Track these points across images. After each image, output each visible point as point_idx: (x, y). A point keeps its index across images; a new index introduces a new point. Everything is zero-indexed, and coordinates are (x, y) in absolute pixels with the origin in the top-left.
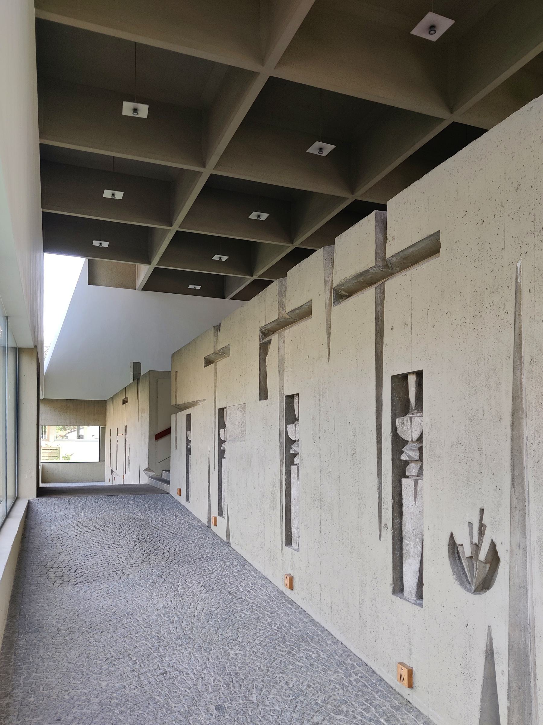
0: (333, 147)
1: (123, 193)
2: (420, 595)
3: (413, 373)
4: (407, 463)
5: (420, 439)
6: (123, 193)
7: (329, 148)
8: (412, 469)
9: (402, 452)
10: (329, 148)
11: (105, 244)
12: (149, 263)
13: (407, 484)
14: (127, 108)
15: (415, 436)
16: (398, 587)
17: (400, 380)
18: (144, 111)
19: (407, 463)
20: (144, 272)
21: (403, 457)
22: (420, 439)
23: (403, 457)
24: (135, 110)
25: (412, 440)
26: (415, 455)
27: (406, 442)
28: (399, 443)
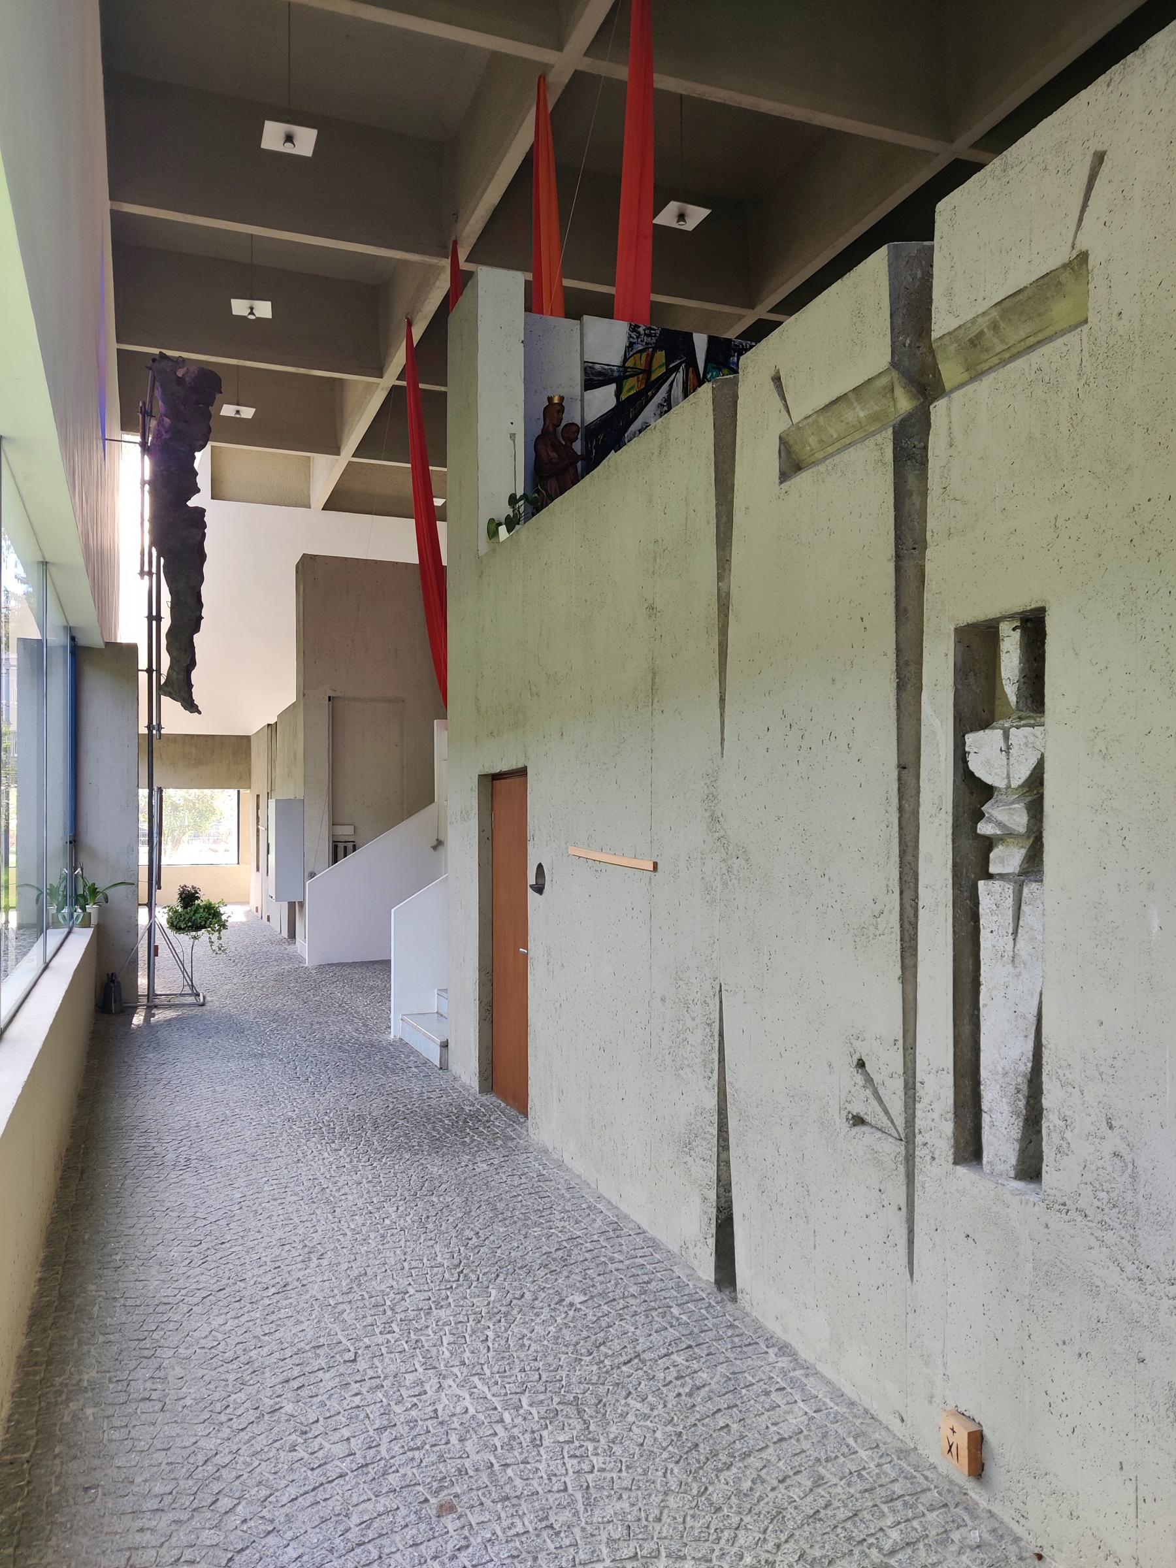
0: (705, 212)
1: (270, 316)
2: (1030, 1169)
3: (1011, 617)
4: (988, 844)
5: (1036, 781)
6: (270, 316)
7: (697, 215)
8: (1007, 859)
9: (981, 816)
10: (697, 215)
11: (248, 413)
12: (335, 450)
13: (993, 899)
14: (272, 136)
15: (1021, 774)
16: (970, 1148)
17: (978, 641)
18: (306, 141)
19: (988, 844)
20: (326, 472)
21: (984, 828)
22: (1036, 781)
23: (984, 828)
24: (289, 138)
25: (1009, 786)
26: (1019, 820)
27: (986, 792)
28: (973, 793)
